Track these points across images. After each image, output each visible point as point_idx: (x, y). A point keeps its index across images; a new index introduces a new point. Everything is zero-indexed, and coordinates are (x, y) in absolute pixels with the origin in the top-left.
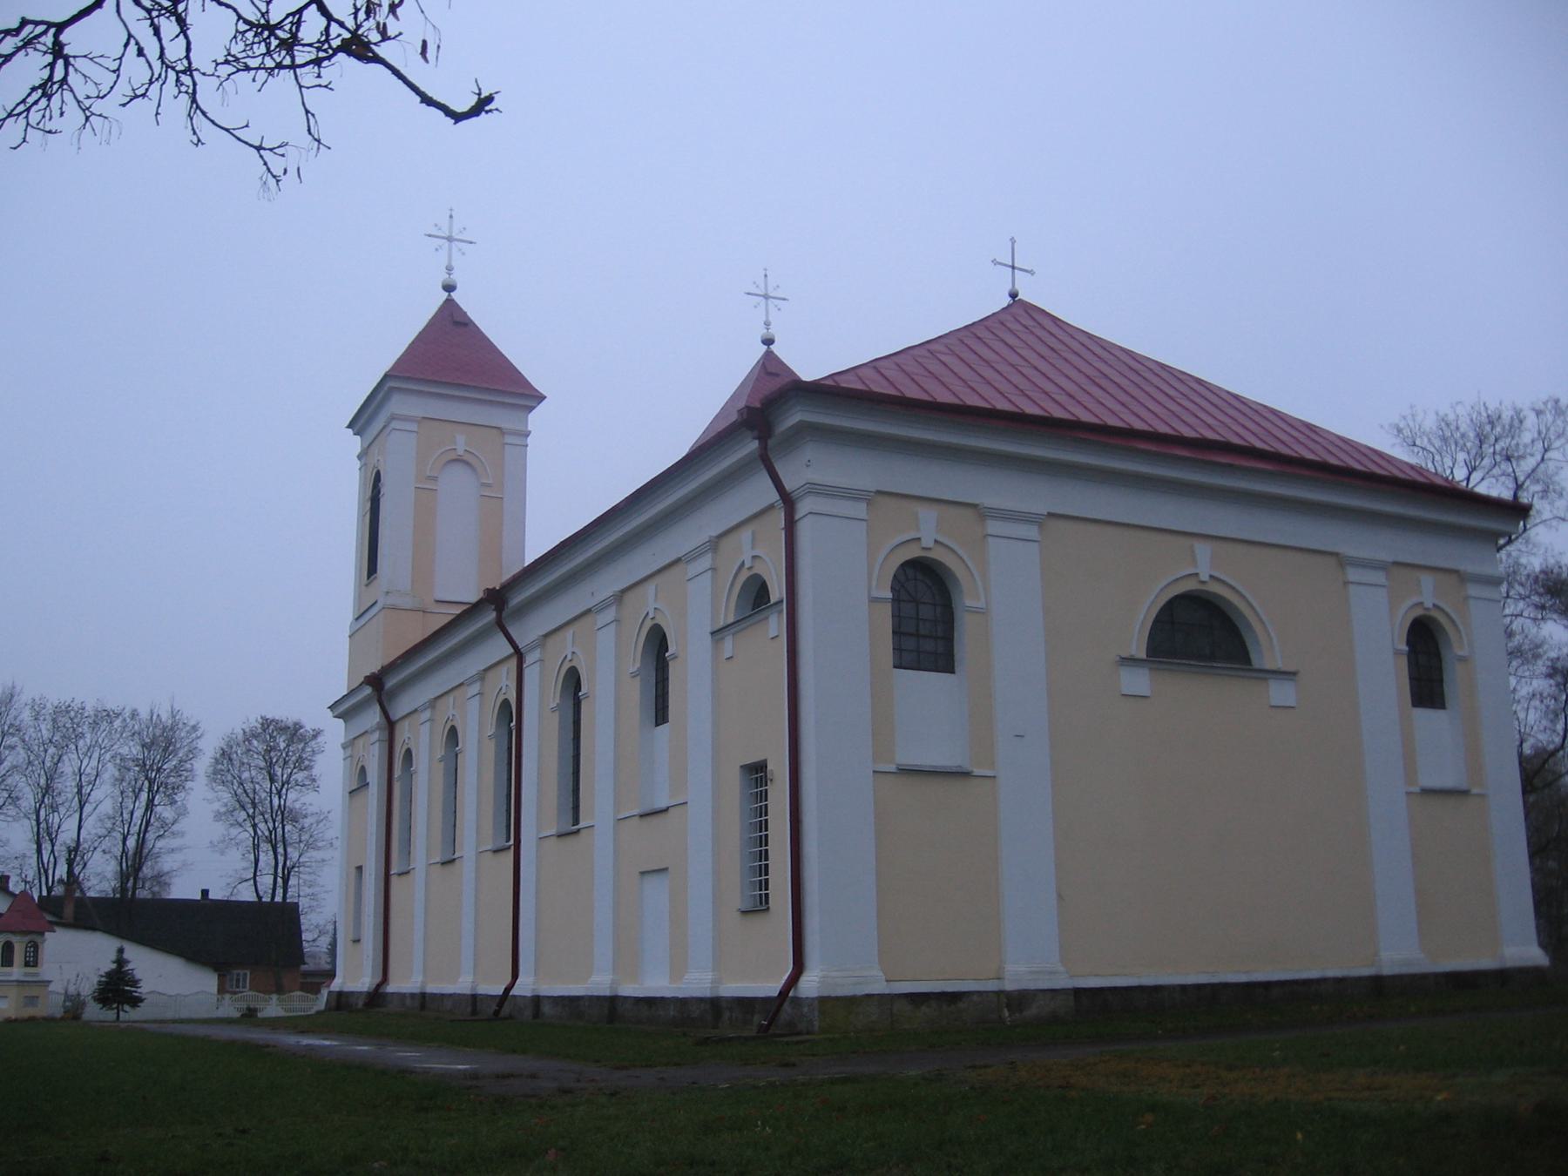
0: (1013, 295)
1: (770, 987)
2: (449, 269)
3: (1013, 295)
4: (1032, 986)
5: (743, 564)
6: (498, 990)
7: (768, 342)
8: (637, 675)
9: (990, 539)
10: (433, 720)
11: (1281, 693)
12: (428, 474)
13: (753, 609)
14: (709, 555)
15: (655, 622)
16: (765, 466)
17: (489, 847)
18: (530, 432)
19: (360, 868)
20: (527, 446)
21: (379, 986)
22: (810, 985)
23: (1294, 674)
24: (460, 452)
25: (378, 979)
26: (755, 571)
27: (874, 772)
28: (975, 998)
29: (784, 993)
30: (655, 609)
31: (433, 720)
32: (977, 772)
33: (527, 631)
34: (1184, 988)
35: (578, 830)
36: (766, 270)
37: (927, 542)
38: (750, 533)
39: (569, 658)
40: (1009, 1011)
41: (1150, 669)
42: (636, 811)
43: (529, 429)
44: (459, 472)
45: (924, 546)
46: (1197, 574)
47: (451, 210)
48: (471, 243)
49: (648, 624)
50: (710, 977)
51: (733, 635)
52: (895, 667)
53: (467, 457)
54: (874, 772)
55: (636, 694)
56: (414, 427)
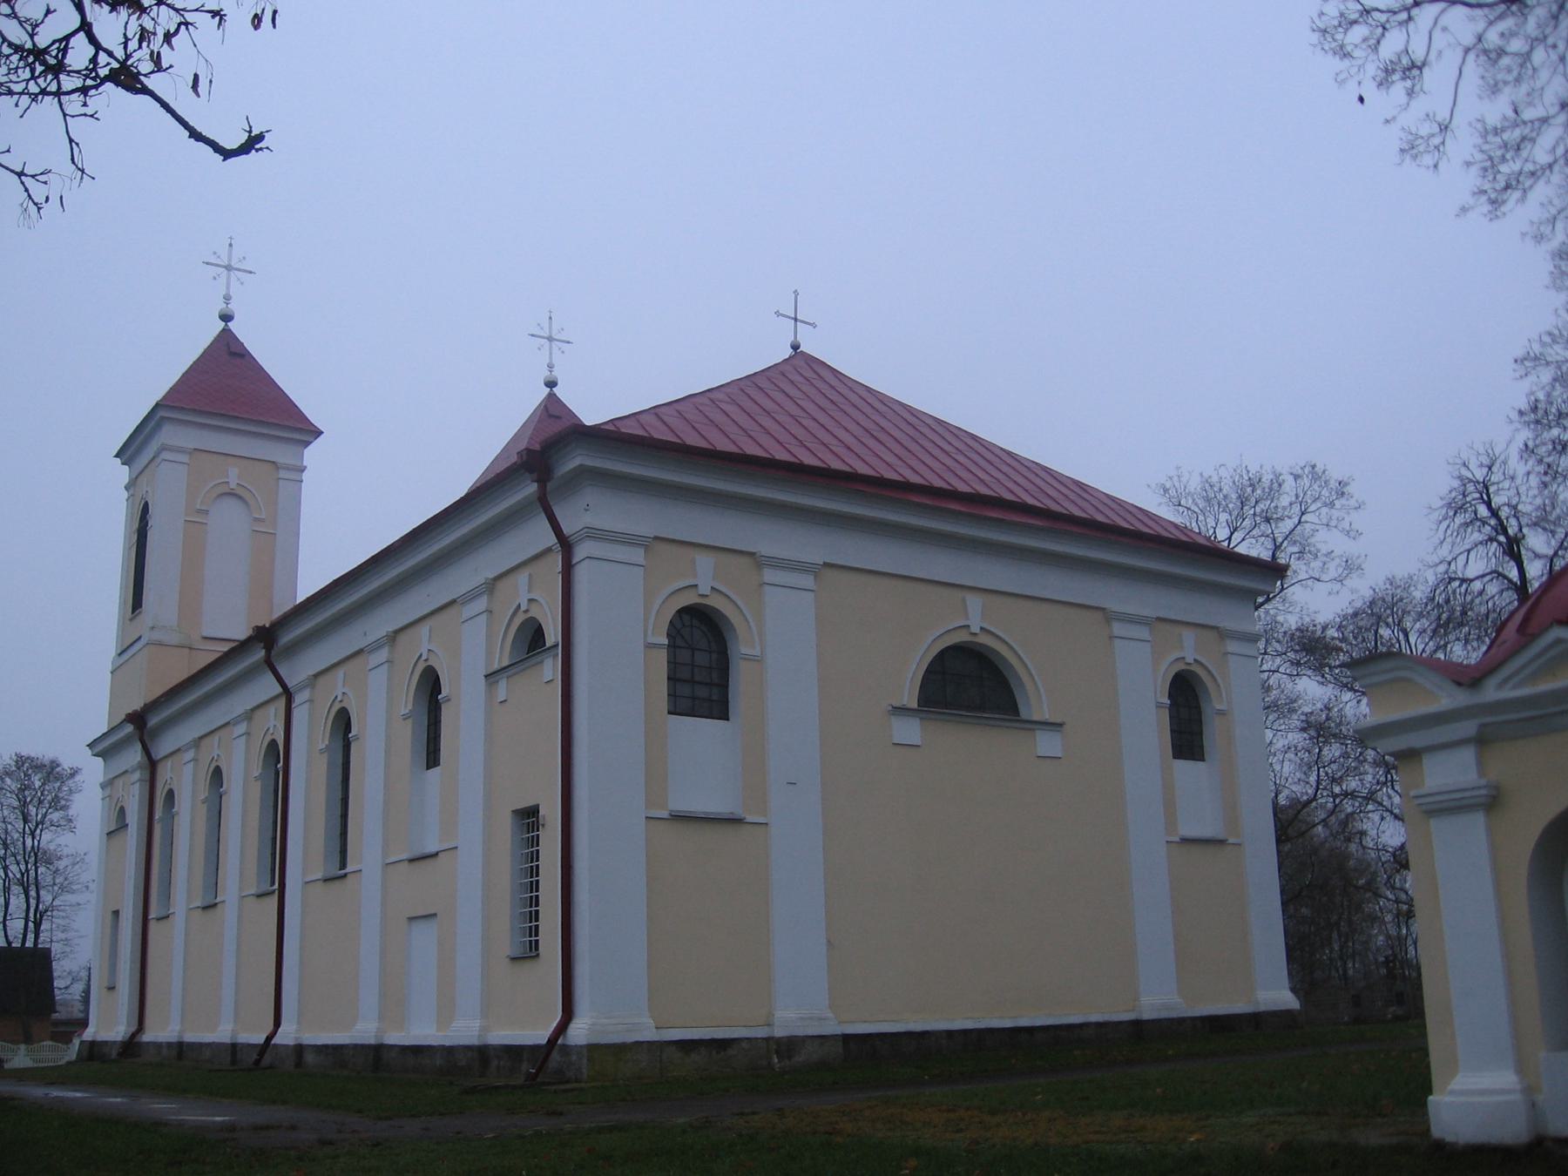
0: (795, 347)
1: (539, 1035)
2: (227, 298)
3: (795, 347)
4: (800, 1032)
5: (519, 606)
6: (259, 1038)
7: (551, 384)
8: (409, 717)
9: (767, 588)
10: (391, 662)
11: (1047, 744)
12: (198, 507)
13: (528, 653)
14: (193, 750)
15: (529, 615)
16: (271, 670)
17: (253, 892)
18: (306, 467)
19: (116, 913)
20: (302, 481)
21: (134, 1035)
22: (579, 1033)
23: (1061, 725)
24: (233, 485)
25: (133, 1029)
26: (429, 663)
27: (647, 818)
28: (744, 1045)
29: (269, 1039)
30: (429, 650)
31: (391, 662)
32: (750, 819)
33: (298, 671)
34: (950, 1034)
35: (345, 875)
36: (550, 312)
37: (704, 589)
38: (526, 574)
39: (271, 731)
40: (777, 1057)
41: (921, 719)
42: (405, 856)
43: (305, 464)
44: (230, 505)
45: (700, 593)
46: (1184, 658)
47: (231, 238)
48: (251, 272)
49: (421, 666)
50: (478, 1025)
51: (508, 678)
52: (669, 713)
53: (240, 491)
54: (647, 818)
55: (407, 736)
56: (184, 458)
